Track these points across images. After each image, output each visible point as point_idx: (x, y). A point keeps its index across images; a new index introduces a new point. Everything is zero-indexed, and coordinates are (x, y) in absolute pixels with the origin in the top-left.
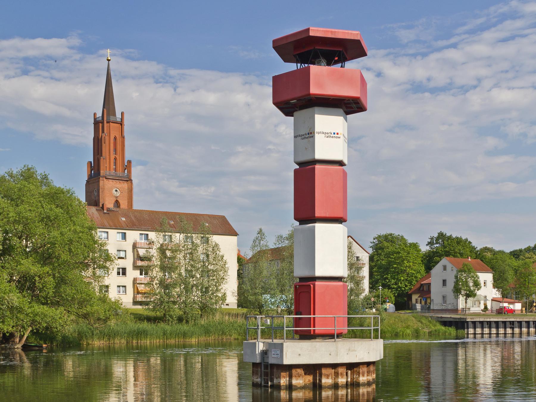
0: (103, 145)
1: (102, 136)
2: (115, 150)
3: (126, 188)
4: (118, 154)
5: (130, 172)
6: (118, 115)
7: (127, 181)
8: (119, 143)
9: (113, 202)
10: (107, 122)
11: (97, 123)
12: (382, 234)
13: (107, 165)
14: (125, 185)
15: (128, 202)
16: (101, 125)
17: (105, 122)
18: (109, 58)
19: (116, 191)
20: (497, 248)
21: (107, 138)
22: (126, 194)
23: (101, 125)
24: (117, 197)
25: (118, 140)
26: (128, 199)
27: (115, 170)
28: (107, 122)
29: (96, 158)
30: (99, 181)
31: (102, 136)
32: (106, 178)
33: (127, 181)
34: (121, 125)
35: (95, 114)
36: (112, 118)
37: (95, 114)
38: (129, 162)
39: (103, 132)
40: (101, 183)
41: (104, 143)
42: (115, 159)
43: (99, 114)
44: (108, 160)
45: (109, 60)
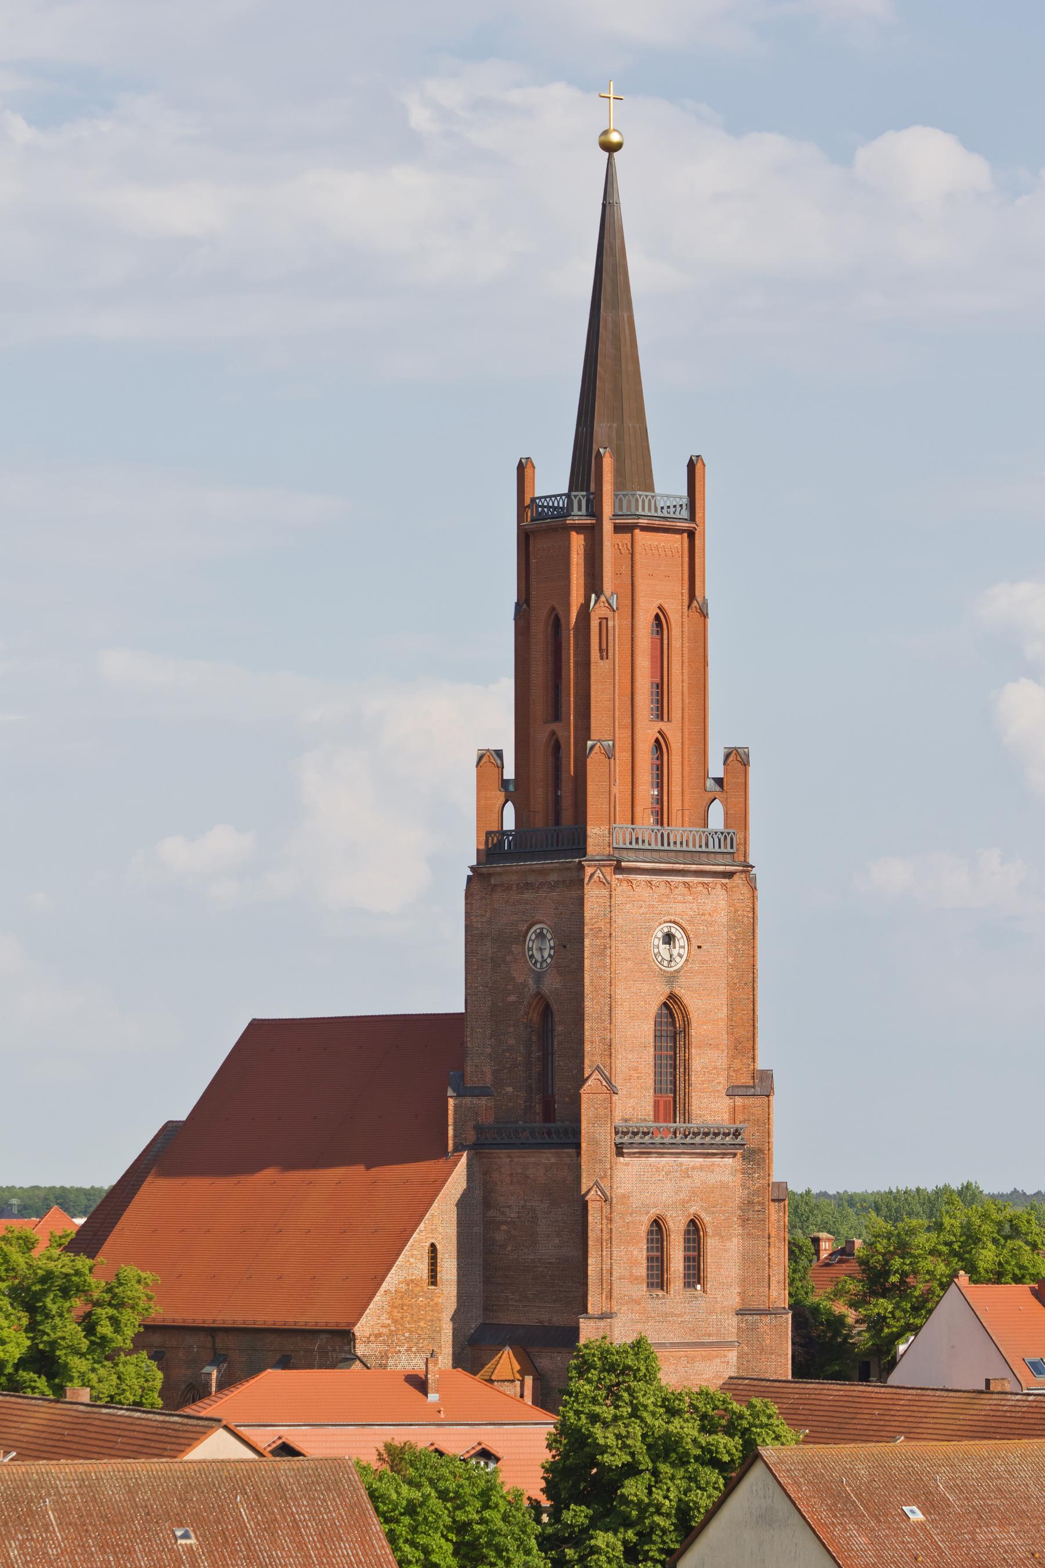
0: (598, 667)
1: (585, 612)
2: (660, 690)
3: (722, 917)
4: (676, 715)
5: (739, 819)
6: (669, 483)
7: (730, 875)
8: (679, 641)
9: (653, 1007)
10: (618, 529)
11: (541, 533)
12: (870, 1191)
13: (620, 789)
14: (715, 902)
15: (732, 1003)
16: (577, 542)
17: (607, 527)
18: (615, 138)
19: (669, 938)
20: (930, 1186)
21: (617, 624)
22: (718, 953)
23: (577, 542)
24: (672, 978)
25: (676, 632)
26: (732, 987)
27: (660, 816)
28: (618, 529)
29: (541, 735)
30: (579, 883)
31: (585, 612)
32: (618, 869)
33: (730, 875)
34: (691, 535)
35: (523, 469)
36: (643, 509)
37: (523, 469)
38: (737, 759)
39: (594, 583)
40: (593, 897)
41: (604, 653)
42: (660, 746)
43: (553, 480)
44: (622, 756)
45: (611, 148)
